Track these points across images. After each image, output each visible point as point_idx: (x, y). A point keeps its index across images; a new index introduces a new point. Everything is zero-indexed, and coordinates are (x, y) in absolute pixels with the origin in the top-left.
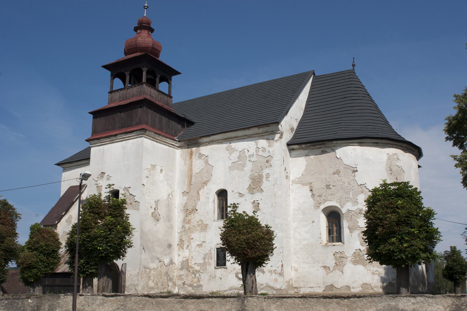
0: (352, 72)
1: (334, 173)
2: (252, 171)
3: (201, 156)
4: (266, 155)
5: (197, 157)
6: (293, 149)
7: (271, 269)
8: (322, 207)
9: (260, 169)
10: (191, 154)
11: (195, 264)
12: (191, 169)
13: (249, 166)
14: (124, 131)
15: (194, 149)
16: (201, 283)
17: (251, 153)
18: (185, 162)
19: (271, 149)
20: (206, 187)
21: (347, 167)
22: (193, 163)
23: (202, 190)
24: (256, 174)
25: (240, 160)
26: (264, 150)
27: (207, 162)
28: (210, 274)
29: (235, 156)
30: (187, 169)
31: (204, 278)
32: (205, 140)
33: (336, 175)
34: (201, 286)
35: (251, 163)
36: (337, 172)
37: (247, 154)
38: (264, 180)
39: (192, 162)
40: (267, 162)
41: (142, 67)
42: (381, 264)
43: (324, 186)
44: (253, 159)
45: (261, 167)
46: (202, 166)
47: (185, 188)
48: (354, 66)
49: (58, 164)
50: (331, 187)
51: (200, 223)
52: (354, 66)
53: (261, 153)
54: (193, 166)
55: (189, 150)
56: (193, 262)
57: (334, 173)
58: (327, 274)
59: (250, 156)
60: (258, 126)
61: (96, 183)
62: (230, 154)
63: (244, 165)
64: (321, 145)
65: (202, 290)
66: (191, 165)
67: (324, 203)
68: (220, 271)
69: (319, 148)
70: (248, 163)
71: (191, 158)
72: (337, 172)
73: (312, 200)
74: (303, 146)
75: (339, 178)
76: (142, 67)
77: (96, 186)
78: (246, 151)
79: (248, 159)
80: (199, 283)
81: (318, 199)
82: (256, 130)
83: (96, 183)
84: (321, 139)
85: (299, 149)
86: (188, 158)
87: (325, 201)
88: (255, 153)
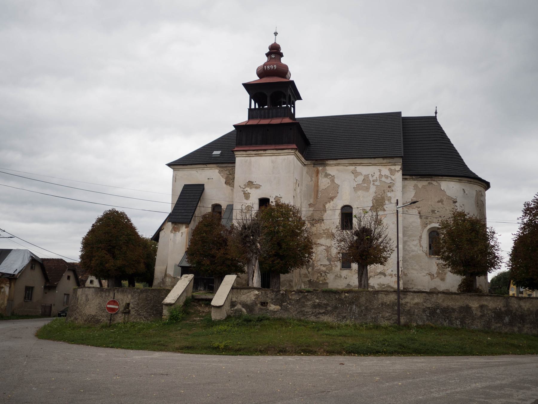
0: (435, 118)
1: (439, 202)
2: (376, 193)
3: (327, 175)
4: (389, 181)
5: (323, 176)
6: (406, 179)
7: (392, 273)
8: (429, 227)
9: (383, 192)
10: (318, 172)
11: (321, 265)
12: (317, 185)
13: (373, 189)
14: (273, 147)
15: (320, 168)
16: (327, 281)
17: (374, 178)
18: (311, 179)
19: (393, 177)
20: (332, 202)
21: (449, 198)
22: (320, 181)
23: (328, 204)
24: (379, 196)
25: (364, 183)
26: (387, 177)
27: (333, 181)
28: (335, 274)
29: (360, 179)
30: (313, 184)
31: (330, 277)
32: (331, 162)
33: (440, 203)
34: (327, 283)
35: (375, 187)
36: (441, 201)
37: (371, 179)
38: (387, 202)
39: (318, 179)
40: (389, 187)
41: (273, 89)
42: (82, 257)
43: (430, 211)
44: (377, 183)
45: (384, 191)
46: (328, 183)
47: (312, 201)
48: (436, 113)
49: (170, 165)
50: (436, 212)
51: (326, 231)
52: (436, 113)
53: (383, 179)
54: (319, 183)
55: (315, 169)
56: (319, 263)
57: (439, 202)
58: (432, 279)
59: (373, 181)
60: (384, 158)
61: (242, 189)
62: (356, 177)
63: (367, 189)
64: (428, 178)
65: (328, 287)
66: (318, 182)
67: (430, 224)
68: (345, 272)
69: (427, 180)
70: (371, 186)
71: (317, 175)
72: (441, 201)
73: (419, 220)
74: (414, 177)
75: (442, 206)
76: (273, 89)
77: (243, 193)
78: (370, 176)
79: (372, 183)
80: (325, 281)
81: (425, 220)
82: (381, 160)
83: (242, 189)
84: (430, 173)
85: (410, 179)
86: (314, 175)
87: (431, 223)
88: (378, 179)
